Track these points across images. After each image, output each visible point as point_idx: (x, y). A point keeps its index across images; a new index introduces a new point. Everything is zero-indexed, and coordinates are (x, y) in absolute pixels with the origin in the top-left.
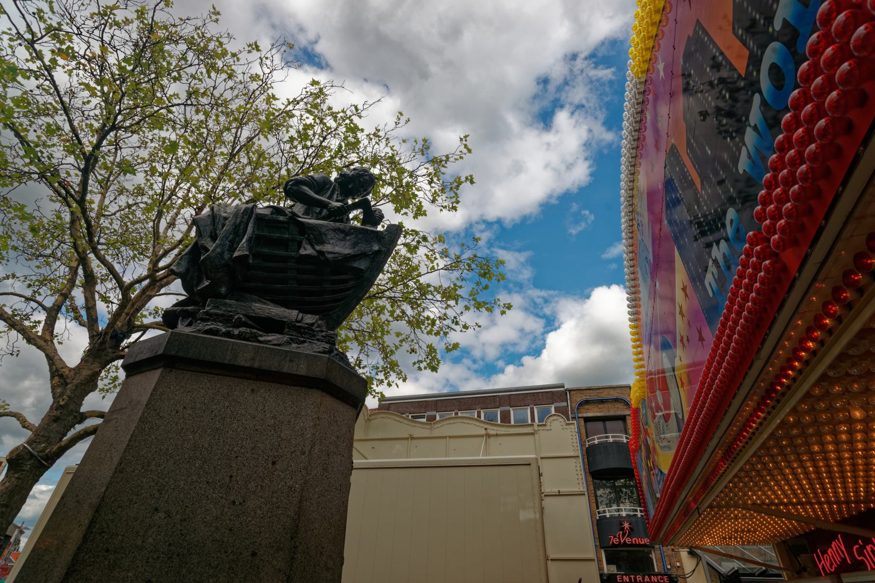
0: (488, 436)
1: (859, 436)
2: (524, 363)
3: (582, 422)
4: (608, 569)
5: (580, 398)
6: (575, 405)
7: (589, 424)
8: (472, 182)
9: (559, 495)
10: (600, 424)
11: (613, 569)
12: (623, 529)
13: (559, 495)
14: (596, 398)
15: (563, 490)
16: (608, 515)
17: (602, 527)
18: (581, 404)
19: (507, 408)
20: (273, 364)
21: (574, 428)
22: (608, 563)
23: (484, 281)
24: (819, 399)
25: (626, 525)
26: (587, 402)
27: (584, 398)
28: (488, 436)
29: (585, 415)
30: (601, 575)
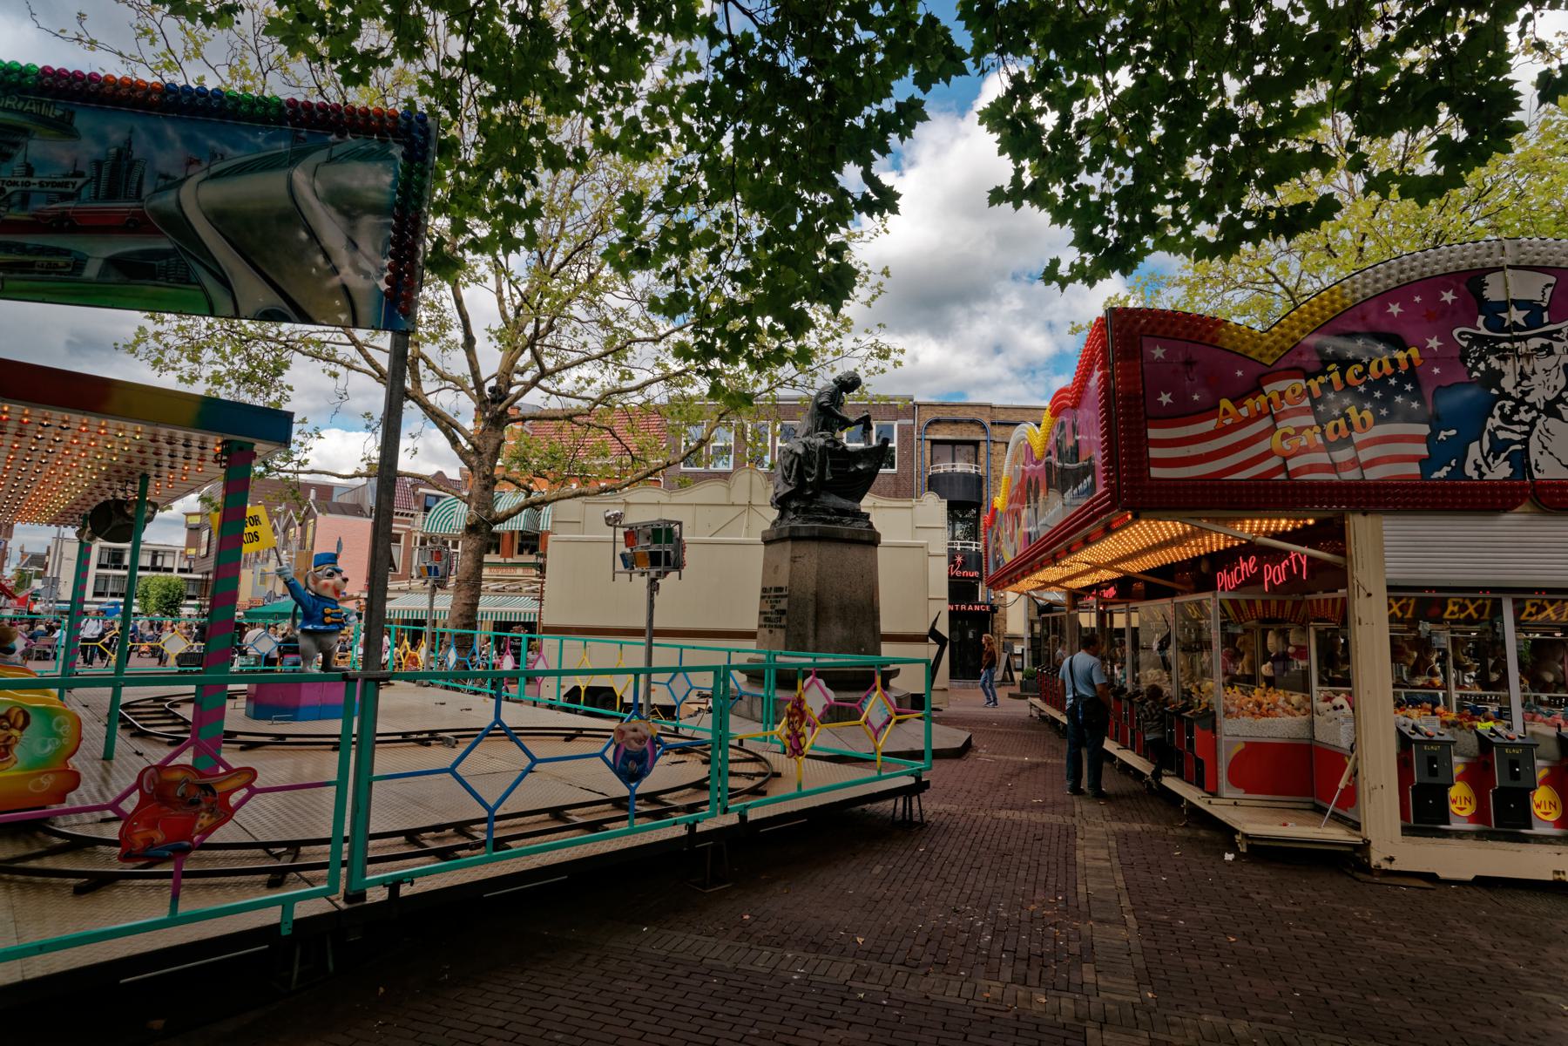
3: (928, 445)
5: (930, 416)
6: (923, 424)
7: (937, 448)
26: (937, 421)
27: (935, 416)
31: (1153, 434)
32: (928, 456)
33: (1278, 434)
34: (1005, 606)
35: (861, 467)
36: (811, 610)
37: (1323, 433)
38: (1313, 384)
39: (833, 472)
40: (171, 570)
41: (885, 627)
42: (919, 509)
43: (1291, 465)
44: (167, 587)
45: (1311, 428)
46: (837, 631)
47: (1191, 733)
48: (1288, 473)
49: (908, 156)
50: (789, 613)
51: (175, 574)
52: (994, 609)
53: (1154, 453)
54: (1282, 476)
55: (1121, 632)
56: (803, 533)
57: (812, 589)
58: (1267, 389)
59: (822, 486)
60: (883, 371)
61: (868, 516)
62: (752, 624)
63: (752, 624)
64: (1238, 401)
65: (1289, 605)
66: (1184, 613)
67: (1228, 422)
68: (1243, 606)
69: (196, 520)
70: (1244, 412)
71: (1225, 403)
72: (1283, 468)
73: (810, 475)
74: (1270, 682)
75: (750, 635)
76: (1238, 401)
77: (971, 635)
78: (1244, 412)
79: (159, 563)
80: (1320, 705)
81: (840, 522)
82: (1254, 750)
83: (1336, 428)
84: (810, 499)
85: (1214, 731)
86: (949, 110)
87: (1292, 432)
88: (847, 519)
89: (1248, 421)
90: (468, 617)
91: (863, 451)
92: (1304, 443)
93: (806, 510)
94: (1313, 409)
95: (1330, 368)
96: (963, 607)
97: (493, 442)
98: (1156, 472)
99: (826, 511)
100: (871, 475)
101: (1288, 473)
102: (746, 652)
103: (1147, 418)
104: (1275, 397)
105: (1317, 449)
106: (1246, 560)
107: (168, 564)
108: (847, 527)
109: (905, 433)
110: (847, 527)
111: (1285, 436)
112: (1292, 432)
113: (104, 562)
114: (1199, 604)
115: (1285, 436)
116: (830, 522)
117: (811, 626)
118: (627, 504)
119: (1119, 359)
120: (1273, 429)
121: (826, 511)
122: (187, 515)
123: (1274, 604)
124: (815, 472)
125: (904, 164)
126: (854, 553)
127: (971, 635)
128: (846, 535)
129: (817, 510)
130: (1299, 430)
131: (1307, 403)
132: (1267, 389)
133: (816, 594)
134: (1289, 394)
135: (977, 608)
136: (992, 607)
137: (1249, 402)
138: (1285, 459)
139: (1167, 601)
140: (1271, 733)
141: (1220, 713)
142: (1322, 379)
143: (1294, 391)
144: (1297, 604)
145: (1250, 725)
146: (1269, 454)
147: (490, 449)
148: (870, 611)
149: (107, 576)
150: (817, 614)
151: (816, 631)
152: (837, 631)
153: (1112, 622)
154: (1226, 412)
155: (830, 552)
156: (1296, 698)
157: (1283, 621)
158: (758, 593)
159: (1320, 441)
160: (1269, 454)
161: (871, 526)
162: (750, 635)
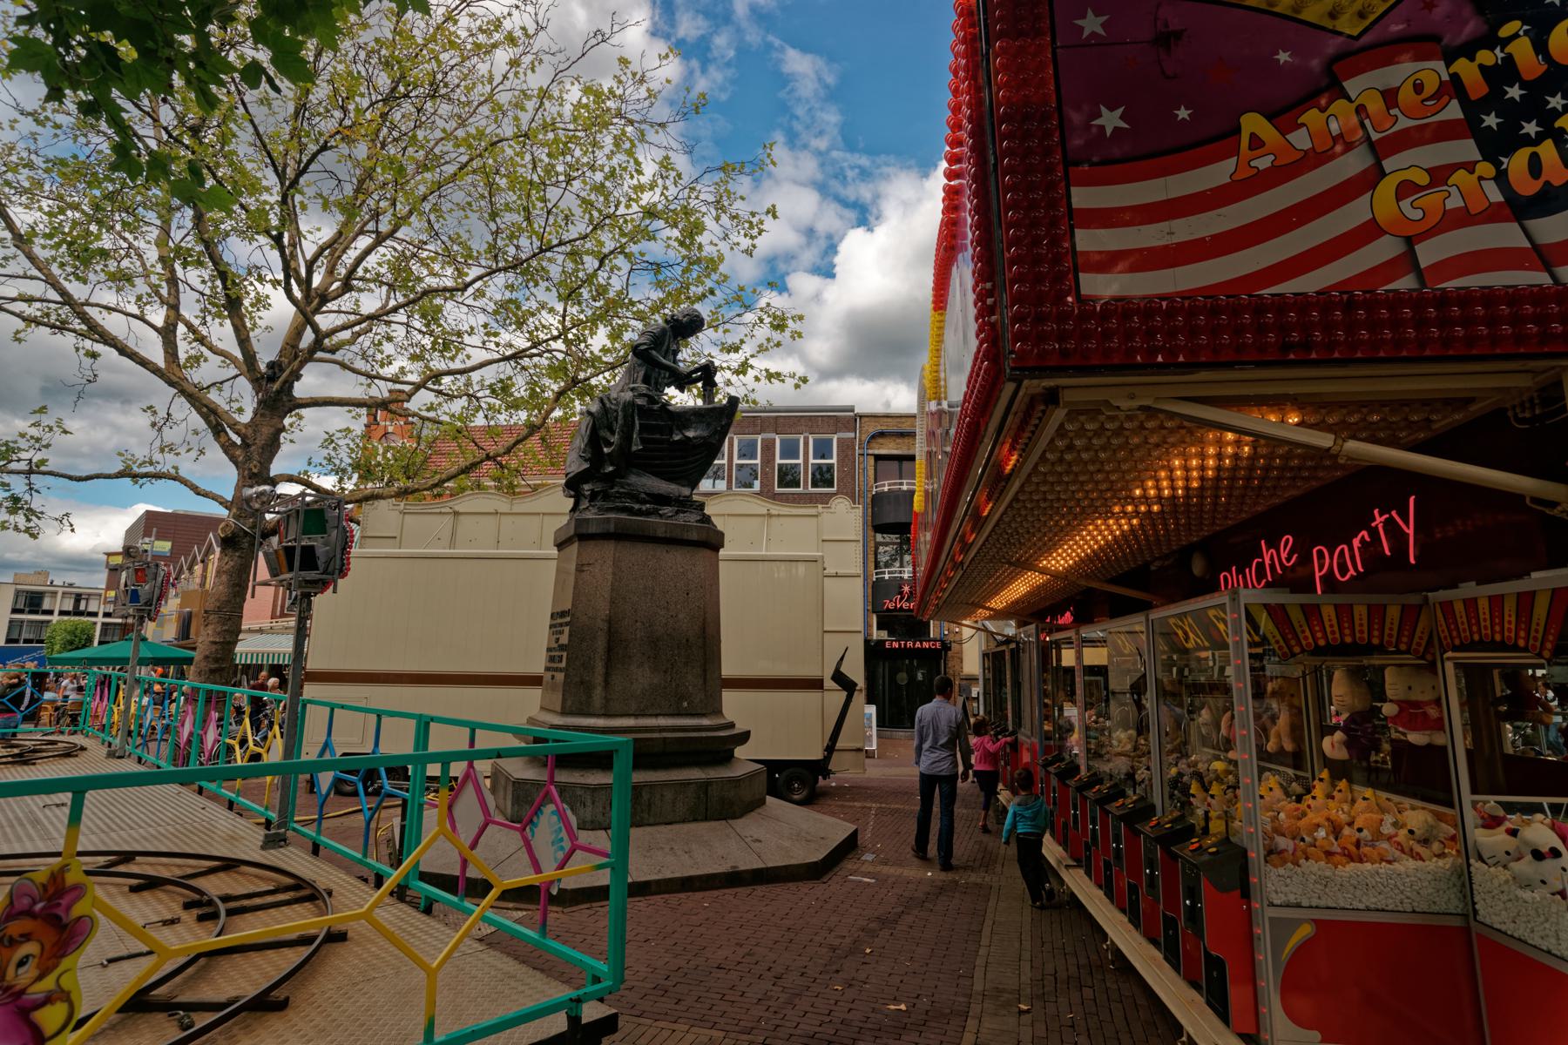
0: (770, 516)
1: (1165, 483)
2: (789, 285)
3: (872, 461)
4: (877, 634)
5: (873, 428)
6: (865, 437)
7: (880, 463)
8: (775, 217)
9: (837, 576)
10: (895, 464)
11: (884, 635)
12: (901, 593)
13: (837, 576)
14: (895, 429)
15: (841, 572)
16: (887, 576)
17: (877, 591)
18: (873, 437)
19: (772, 435)
20: (677, 534)
21: (859, 511)
22: (879, 628)
23: (777, 336)
24: (1153, 431)
25: (906, 589)
26: (882, 434)
27: (879, 428)
28: (770, 516)
29: (876, 452)
30: (867, 642)
31: (1082, 197)
32: (871, 473)
33: (1387, 187)
34: (960, 643)
35: (691, 434)
36: (601, 643)
37: (1501, 178)
38: (1462, 66)
39: (643, 441)
40: (95, 614)
41: (728, 670)
42: (826, 517)
43: (1427, 254)
44: (73, 633)
45: (1470, 167)
46: (642, 677)
47: (1193, 893)
48: (1420, 274)
49: (875, 211)
50: (591, 653)
51: (55, 618)
52: (946, 647)
53: (1087, 240)
54: (1405, 283)
55: (1070, 671)
56: (593, 530)
57: (603, 609)
58: (1352, 86)
59: (627, 461)
60: (778, 345)
61: (701, 506)
62: (538, 666)
63: (538, 666)
64: (1283, 115)
65: (1393, 613)
66: (1169, 635)
67: (1264, 163)
68: (1296, 616)
69: (119, 560)
70: (1300, 140)
71: (1253, 123)
72: (1407, 261)
73: (609, 444)
74: (1339, 771)
75: (534, 681)
76: (1283, 115)
77: (920, 677)
78: (1300, 140)
79: (82, 607)
80: (1484, 838)
81: (654, 513)
82: (1334, 934)
83: (1535, 165)
84: (610, 479)
85: (1246, 894)
86: (909, 167)
87: (1423, 179)
88: (667, 510)
89: (1314, 159)
90: (216, 660)
91: (695, 412)
92: (1454, 202)
93: (606, 497)
94: (1470, 127)
95: (1505, 32)
96: (910, 644)
97: (266, 431)
98: (1101, 286)
99: (634, 497)
100: (711, 449)
101: (1420, 274)
102: (526, 706)
103: (1069, 162)
104: (1375, 105)
105: (1492, 215)
106: (1274, 544)
107: (92, 608)
108: (665, 520)
109: (846, 447)
110: (665, 520)
111: (1406, 190)
112: (1423, 179)
113: (20, 606)
114: (1200, 615)
115: (1406, 190)
116: (640, 513)
117: (600, 667)
118: (456, 514)
119: (1001, 35)
120: (1375, 175)
121: (634, 497)
122: (109, 554)
123: (1360, 612)
124: (615, 439)
125: (872, 219)
126: (675, 561)
127: (920, 677)
128: (660, 533)
129: (621, 496)
130: (1439, 176)
131: (1454, 111)
132: (1352, 86)
133: (609, 621)
134: (1406, 95)
135: (926, 645)
136: (943, 642)
137: (1311, 117)
138: (1410, 241)
139: (1140, 618)
140: (1372, 900)
141: (1256, 854)
142: (1486, 57)
143: (1418, 88)
144: (1410, 615)
145: (1326, 882)
146: (1370, 231)
147: (260, 441)
148: (704, 641)
149: (22, 622)
150: (609, 650)
151: (607, 675)
152: (642, 677)
153: (1059, 659)
154: (1256, 142)
155: (636, 555)
156: (1417, 816)
157: (1369, 649)
158: (548, 621)
159: (1495, 195)
160: (1370, 231)
161: (706, 519)
162: (534, 681)
